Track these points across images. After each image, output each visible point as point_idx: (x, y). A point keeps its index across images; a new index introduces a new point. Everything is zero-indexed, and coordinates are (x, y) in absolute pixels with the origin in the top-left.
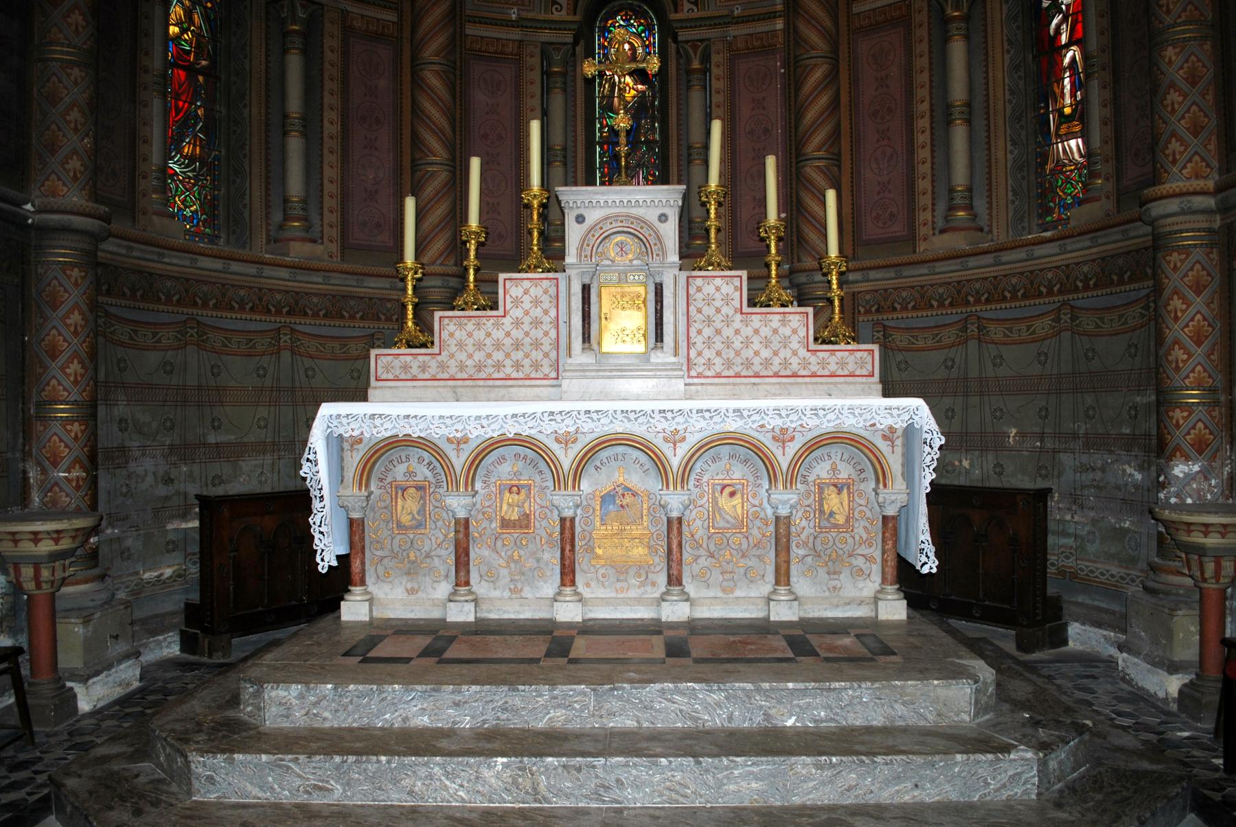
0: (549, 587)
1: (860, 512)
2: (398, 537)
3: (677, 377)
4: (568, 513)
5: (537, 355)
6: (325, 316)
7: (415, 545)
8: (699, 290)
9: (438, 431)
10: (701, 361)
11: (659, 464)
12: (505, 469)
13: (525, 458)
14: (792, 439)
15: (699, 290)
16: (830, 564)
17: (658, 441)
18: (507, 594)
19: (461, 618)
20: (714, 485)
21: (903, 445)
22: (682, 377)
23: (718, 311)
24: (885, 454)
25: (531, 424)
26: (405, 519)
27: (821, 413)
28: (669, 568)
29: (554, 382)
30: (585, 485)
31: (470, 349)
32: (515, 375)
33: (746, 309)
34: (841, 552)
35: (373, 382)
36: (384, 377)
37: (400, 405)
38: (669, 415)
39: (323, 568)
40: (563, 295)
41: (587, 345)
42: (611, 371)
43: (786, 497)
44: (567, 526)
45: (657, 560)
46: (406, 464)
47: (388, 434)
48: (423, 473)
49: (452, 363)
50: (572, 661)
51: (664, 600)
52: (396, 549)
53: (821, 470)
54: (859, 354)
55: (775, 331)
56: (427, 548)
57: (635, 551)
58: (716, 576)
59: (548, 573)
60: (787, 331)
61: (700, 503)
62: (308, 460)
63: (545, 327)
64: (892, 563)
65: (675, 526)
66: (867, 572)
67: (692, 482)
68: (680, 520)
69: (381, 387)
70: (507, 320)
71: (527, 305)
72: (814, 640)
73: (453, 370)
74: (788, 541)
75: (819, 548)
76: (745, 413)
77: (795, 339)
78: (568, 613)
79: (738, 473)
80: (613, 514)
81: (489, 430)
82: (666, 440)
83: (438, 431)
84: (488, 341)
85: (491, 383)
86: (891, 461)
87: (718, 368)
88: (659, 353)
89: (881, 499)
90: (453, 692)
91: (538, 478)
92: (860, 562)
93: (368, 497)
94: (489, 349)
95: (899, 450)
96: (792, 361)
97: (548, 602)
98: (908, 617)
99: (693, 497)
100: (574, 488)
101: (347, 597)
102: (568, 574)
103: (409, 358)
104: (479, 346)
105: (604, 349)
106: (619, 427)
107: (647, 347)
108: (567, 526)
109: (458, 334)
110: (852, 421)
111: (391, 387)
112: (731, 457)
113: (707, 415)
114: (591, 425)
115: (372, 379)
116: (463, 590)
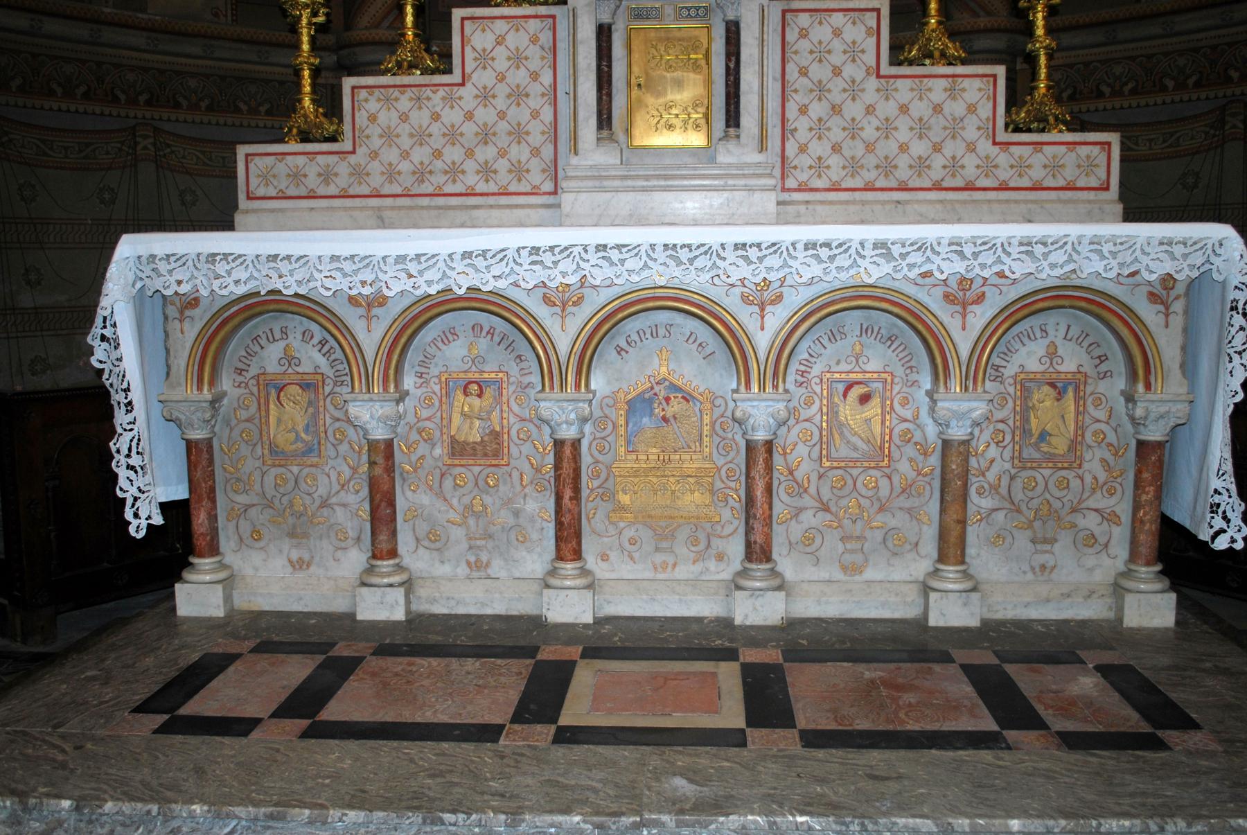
0: (536, 558)
1: (1095, 433)
2: (274, 471)
3: (764, 189)
4: (568, 433)
5: (519, 152)
6: (210, 109)
7: (303, 486)
8: (804, 34)
9: (328, 283)
10: (805, 161)
11: (733, 344)
12: (455, 355)
13: (491, 332)
14: (980, 298)
15: (804, 34)
16: (1037, 524)
17: (732, 302)
18: (462, 570)
19: (381, 615)
20: (831, 382)
21: (1186, 312)
22: (774, 189)
23: (837, 71)
24: (1152, 328)
25: (496, 271)
26: (283, 439)
27: (1039, 250)
28: (749, 530)
29: (550, 200)
30: (598, 382)
31: (406, 142)
32: (481, 187)
33: (886, 69)
34: (1057, 504)
35: (243, 203)
36: (261, 192)
37: (296, 242)
38: (753, 253)
39: (138, 529)
40: (563, 46)
41: (605, 133)
42: (647, 178)
43: (965, 406)
44: (566, 456)
45: (726, 514)
46: (282, 344)
47: (241, 290)
48: (312, 359)
49: (375, 167)
50: (568, 736)
51: (738, 588)
52: (270, 492)
53: (1028, 357)
54: (1083, 151)
55: (938, 109)
56: (322, 491)
57: (688, 498)
58: (832, 544)
59: (535, 536)
60: (958, 108)
61: (805, 414)
62: (103, 338)
63: (534, 102)
64: (1151, 526)
65: (760, 455)
66: (1102, 540)
67: (791, 378)
68: (769, 445)
69: (255, 211)
70: (468, 92)
71: (501, 64)
72: (1025, 679)
73: (376, 181)
74: (965, 485)
75: (1018, 495)
76: (896, 250)
77: (971, 123)
78: (569, 608)
79: (876, 360)
80: (649, 434)
81: (421, 281)
82: (745, 299)
83: (328, 283)
84: (435, 128)
85: (441, 201)
86: (1162, 342)
87: (835, 174)
88: (731, 145)
89: (1139, 412)
90: (311, 822)
91: (514, 369)
92: (1090, 522)
93: (215, 402)
94: (437, 142)
95: (1177, 321)
96: (965, 161)
97: (535, 587)
98: (1177, 623)
99: (794, 403)
100: (578, 386)
101: (186, 575)
102: (568, 540)
103: (301, 160)
104: (421, 137)
105: (637, 142)
106: (661, 275)
107: (709, 137)
108: (566, 456)
109: (383, 118)
110: (1099, 266)
111: (273, 211)
112: (865, 331)
113: (824, 253)
114: (609, 272)
115: (242, 196)
116: (385, 565)
